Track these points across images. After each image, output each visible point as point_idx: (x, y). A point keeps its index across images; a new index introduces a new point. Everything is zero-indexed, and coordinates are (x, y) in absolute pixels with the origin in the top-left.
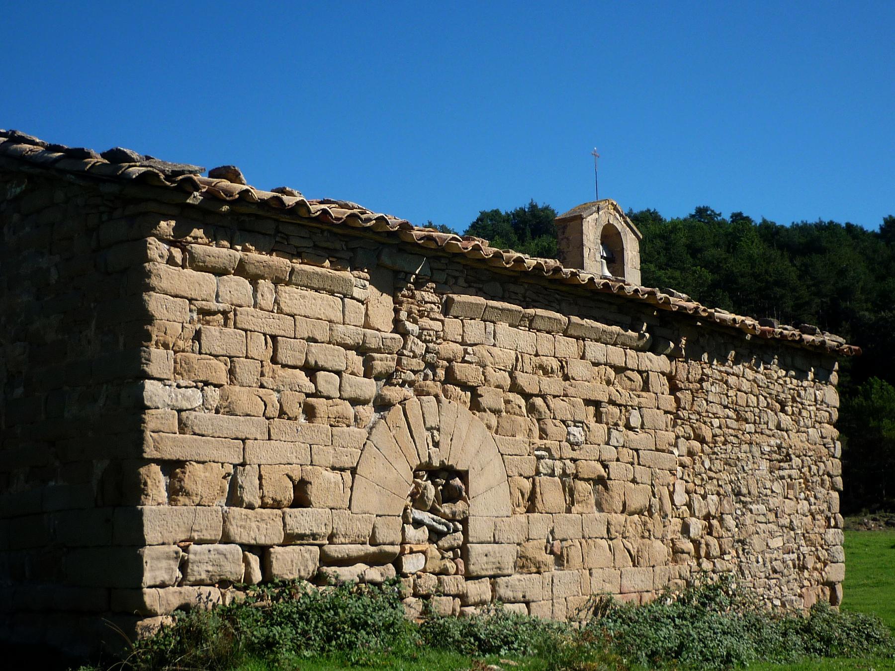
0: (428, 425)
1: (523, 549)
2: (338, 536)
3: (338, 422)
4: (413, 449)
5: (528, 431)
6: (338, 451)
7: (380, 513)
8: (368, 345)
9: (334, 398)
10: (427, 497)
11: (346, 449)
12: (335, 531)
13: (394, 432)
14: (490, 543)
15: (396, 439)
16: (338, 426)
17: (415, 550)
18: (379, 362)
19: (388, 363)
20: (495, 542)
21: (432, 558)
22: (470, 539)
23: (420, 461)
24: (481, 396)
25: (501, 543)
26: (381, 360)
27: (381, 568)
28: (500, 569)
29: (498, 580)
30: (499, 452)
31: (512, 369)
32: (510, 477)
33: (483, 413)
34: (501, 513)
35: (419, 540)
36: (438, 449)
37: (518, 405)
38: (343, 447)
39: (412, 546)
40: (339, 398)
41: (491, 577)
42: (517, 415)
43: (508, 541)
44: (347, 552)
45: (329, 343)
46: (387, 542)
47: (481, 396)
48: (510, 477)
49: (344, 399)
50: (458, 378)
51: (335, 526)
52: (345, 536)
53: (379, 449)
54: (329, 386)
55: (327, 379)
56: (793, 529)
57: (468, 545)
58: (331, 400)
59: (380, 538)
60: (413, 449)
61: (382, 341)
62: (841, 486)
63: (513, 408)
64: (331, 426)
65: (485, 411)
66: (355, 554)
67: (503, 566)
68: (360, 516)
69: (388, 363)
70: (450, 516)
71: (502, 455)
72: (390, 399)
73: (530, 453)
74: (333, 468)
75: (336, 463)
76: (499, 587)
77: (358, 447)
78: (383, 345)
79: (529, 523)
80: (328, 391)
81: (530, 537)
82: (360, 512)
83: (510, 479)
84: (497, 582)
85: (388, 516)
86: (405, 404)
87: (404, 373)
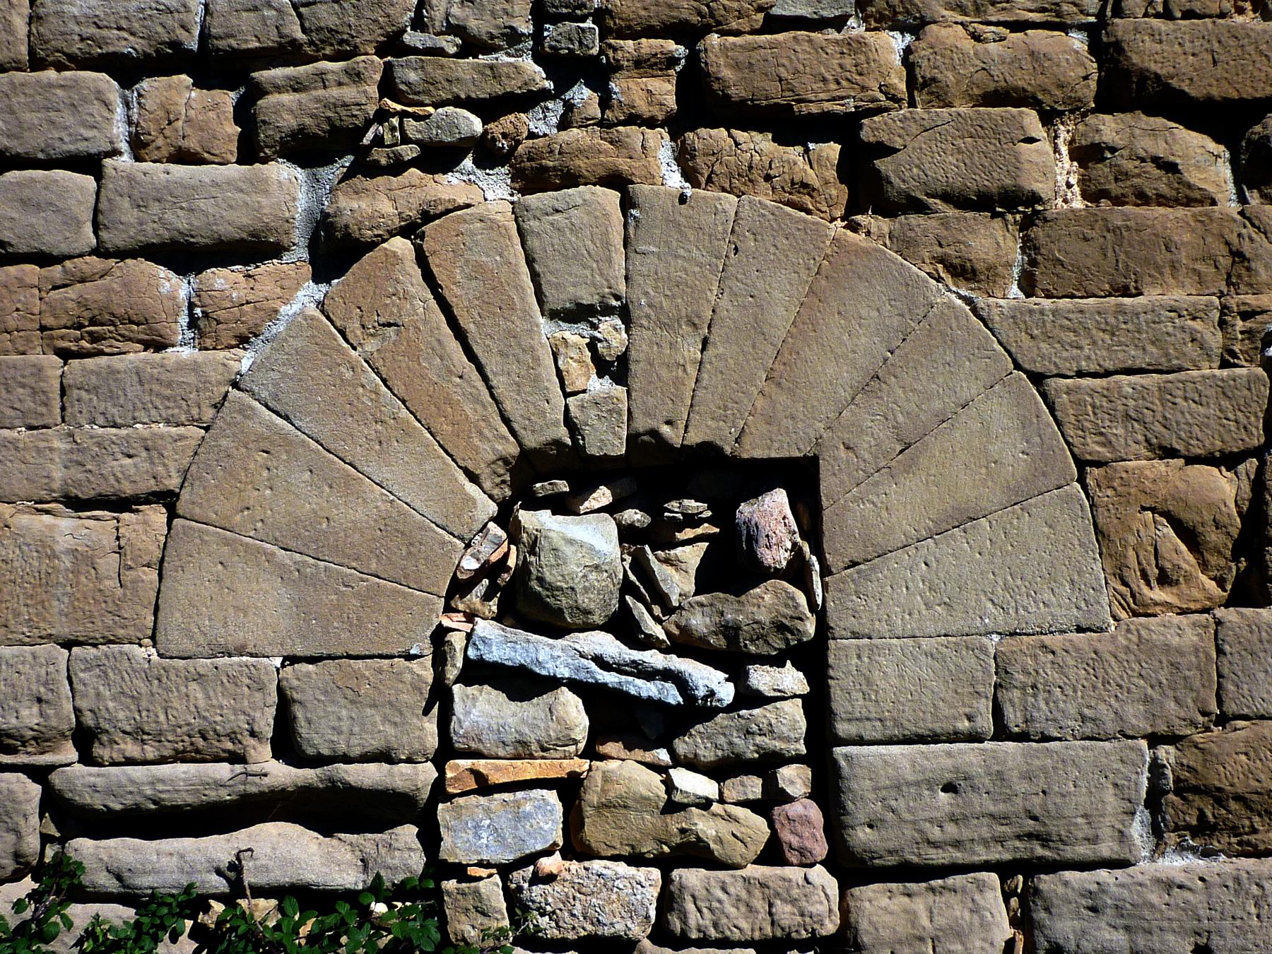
0: (557, 299)
1: (1192, 758)
2: (105, 738)
3: (95, 338)
4: (477, 400)
5: (1225, 262)
6: (88, 443)
7: (299, 650)
8: (221, 44)
9: (70, 257)
10: (541, 580)
11: (124, 432)
12: (89, 720)
13: (371, 346)
14: (974, 737)
15: (378, 374)
16: (101, 353)
17: (496, 778)
18: (287, 98)
19: (335, 92)
20: (1002, 732)
21: (607, 806)
22: (843, 728)
23: (520, 444)
24: (885, 150)
25: (1046, 738)
26: (297, 86)
27: (367, 841)
28: (1044, 840)
29: (1046, 882)
30: (1018, 366)
31: (1101, 15)
32: (1098, 464)
33: (914, 219)
34: (1035, 615)
35: (524, 744)
36: (620, 391)
37: (1156, 160)
38: (115, 426)
39: (481, 764)
40: (96, 252)
41: (1004, 870)
42: (1162, 200)
43: (1089, 729)
44: (149, 792)
45: (37, 63)
46: (356, 751)
47: (885, 150)
48: (1098, 464)
49: (122, 254)
50: (736, 92)
51: (83, 704)
52: (138, 734)
53: (287, 418)
54: (36, 220)
55: (26, 193)
56: (170, 124)
57: (839, 751)
58: (59, 267)
59: (315, 737)
60: (477, 400)
61: (300, 16)
62: (646, 855)
63: (1121, 175)
64: (65, 355)
65: (919, 207)
66: (185, 798)
67: (1054, 828)
68: (204, 664)
69: (335, 92)
70: (718, 642)
71: (1037, 379)
72: (347, 226)
73: (1233, 354)
74: (77, 504)
75: (77, 483)
76: (1047, 910)
77: (183, 418)
78: (304, 30)
79: (1220, 651)
80: (36, 235)
81: (1231, 708)
82: (207, 651)
83: (1093, 474)
84: (1037, 892)
85: (350, 657)
86: (422, 236)
87: (417, 118)
